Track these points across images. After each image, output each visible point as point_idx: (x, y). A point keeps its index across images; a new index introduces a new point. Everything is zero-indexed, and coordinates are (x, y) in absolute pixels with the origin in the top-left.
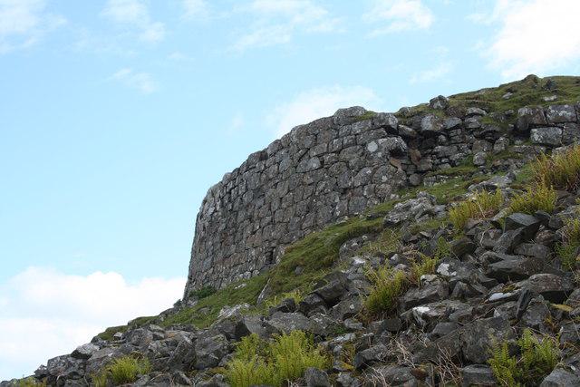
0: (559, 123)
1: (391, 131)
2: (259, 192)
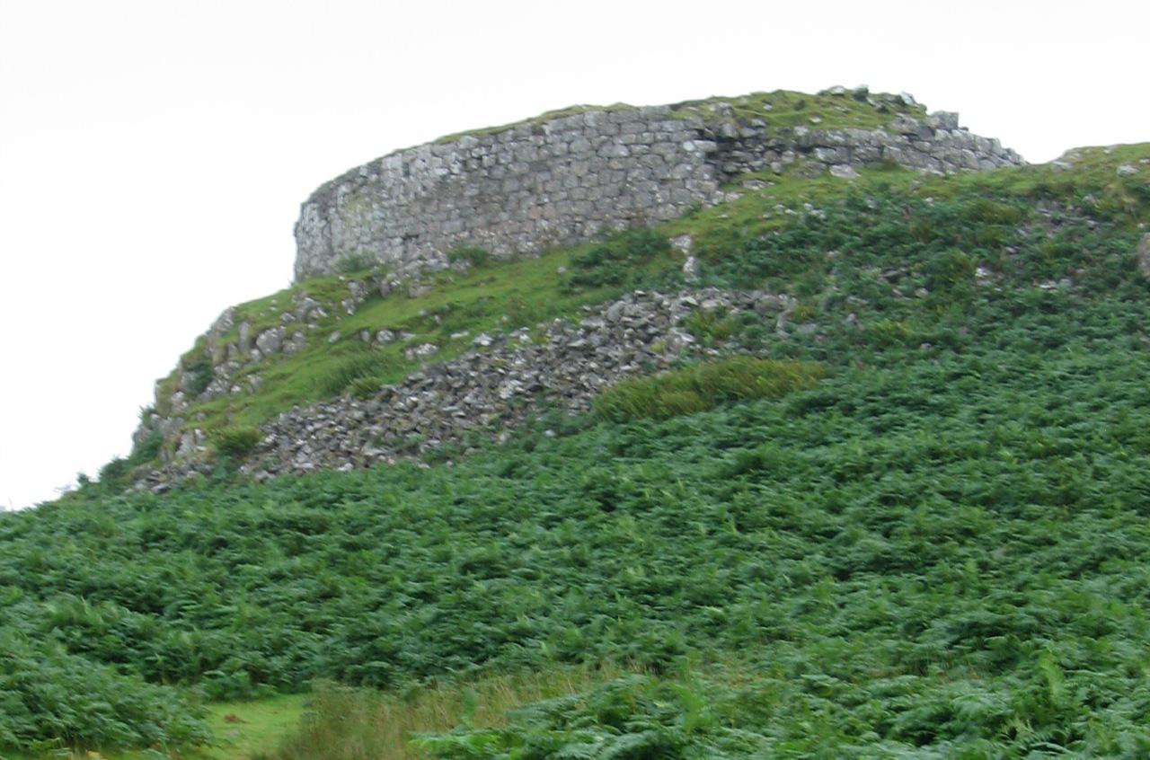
0: (834, 146)
1: (702, 135)
2: (539, 166)
